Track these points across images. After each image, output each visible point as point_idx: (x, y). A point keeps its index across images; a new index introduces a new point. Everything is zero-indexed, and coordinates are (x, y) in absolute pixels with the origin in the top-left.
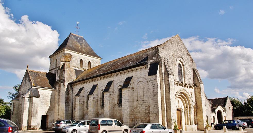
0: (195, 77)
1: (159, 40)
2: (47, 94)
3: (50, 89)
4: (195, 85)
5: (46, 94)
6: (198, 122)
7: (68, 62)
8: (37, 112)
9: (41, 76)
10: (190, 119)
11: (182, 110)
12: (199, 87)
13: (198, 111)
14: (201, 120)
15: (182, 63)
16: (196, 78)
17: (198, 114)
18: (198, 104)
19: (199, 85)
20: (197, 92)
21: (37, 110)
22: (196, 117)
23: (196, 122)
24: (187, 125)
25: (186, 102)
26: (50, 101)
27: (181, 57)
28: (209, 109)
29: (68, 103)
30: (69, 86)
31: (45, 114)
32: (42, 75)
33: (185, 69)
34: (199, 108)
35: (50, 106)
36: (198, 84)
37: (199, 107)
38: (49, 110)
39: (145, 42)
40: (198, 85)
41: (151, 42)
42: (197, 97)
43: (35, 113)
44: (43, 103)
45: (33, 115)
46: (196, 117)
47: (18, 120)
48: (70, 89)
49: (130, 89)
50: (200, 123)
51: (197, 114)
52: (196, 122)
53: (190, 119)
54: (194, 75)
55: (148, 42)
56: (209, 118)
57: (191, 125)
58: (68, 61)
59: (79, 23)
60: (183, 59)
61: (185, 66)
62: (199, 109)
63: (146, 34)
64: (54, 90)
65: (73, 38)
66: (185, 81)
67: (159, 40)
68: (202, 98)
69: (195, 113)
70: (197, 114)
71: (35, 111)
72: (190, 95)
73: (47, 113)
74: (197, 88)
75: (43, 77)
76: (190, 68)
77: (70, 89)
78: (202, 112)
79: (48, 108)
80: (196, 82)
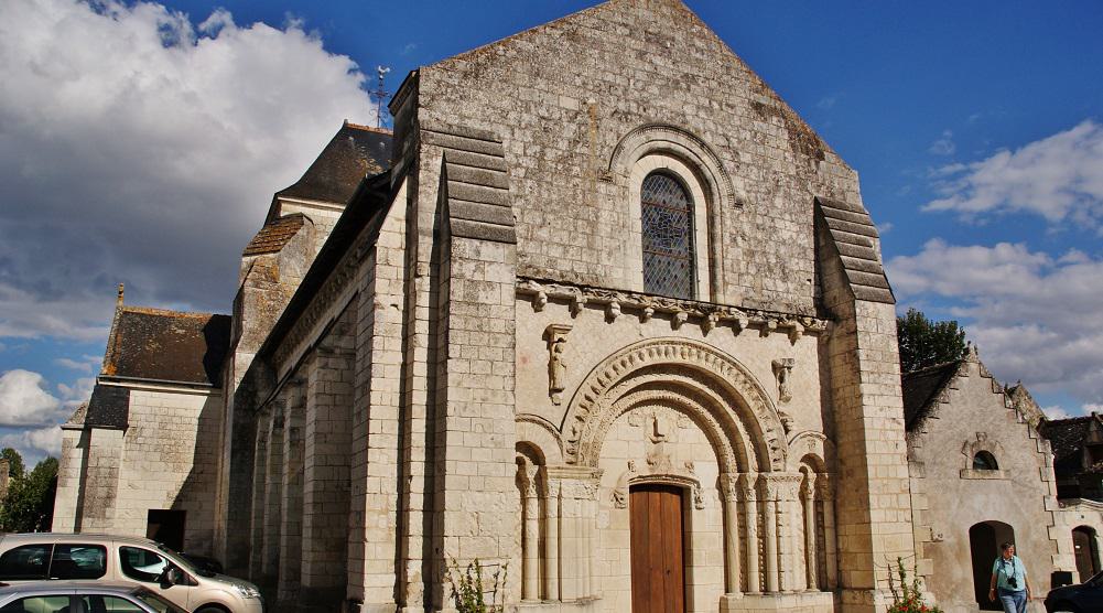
0: (830, 257)
1: (1013, 153)
2: (182, 412)
3: (192, 387)
4: (824, 308)
5: (171, 412)
6: (845, 575)
7: (271, 255)
8: (110, 497)
9: (180, 331)
10: (764, 554)
11: (693, 487)
12: (851, 321)
13: (843, 493)
14: (860, 559)
15: (696, 169)
16: (833, 263)
17: (844, 515)
18: (846, 448)
19: (847, 310)
20: (838, 361)
21: (110, 487)
22: (829, 534)
23: (831, 573)
24: (737, 594)
25: (731, 433)
26: (192, 443)
27: (677, 123)
28: (1034, 475)
29: (247, 454)
30: (260, 369)
31: (164, 503)
32: (181, 328)
33: (724, 204)
34: (851, 473)
35: (194, 468)
36: (842, 306)
37: (849, 463)
38: (189, 486)
39: (948, 169)
40: (842, 308)
41: (975, 165)
42: (841, 393)
43: (99, 502)
44: (157, 456)
45: (91, 508)
46: (829, 534)
47: (954, 507)
48: (260, 381)
49: (331, 360)
50: (854, 578)
51: (841, 518)
52: (831, 573)
53: (764, 554)
54: (822, 243)
55: (960, 167)
56: (1026, 535)
57: (766, 590)
58: (270, 252)
59: (388, 70)
60: (708, 138)
61: (720, 186)
62: (849, 483)
63: (947, 133)
64: (216, 392)
65: (353, 144)
66: (713, 289)
67: (1013, 153)
68: (865, 400)
69: (827, 508)
70: (836, 517)
71: (102, 492)
72: (769, 383)
73: (179, 499)
74: (838, 331)
75: (184, 336)
76: (779, 202)
77: (260, 382)
78: (865, 503)
79: (181, 477)
80: (835, 290)
